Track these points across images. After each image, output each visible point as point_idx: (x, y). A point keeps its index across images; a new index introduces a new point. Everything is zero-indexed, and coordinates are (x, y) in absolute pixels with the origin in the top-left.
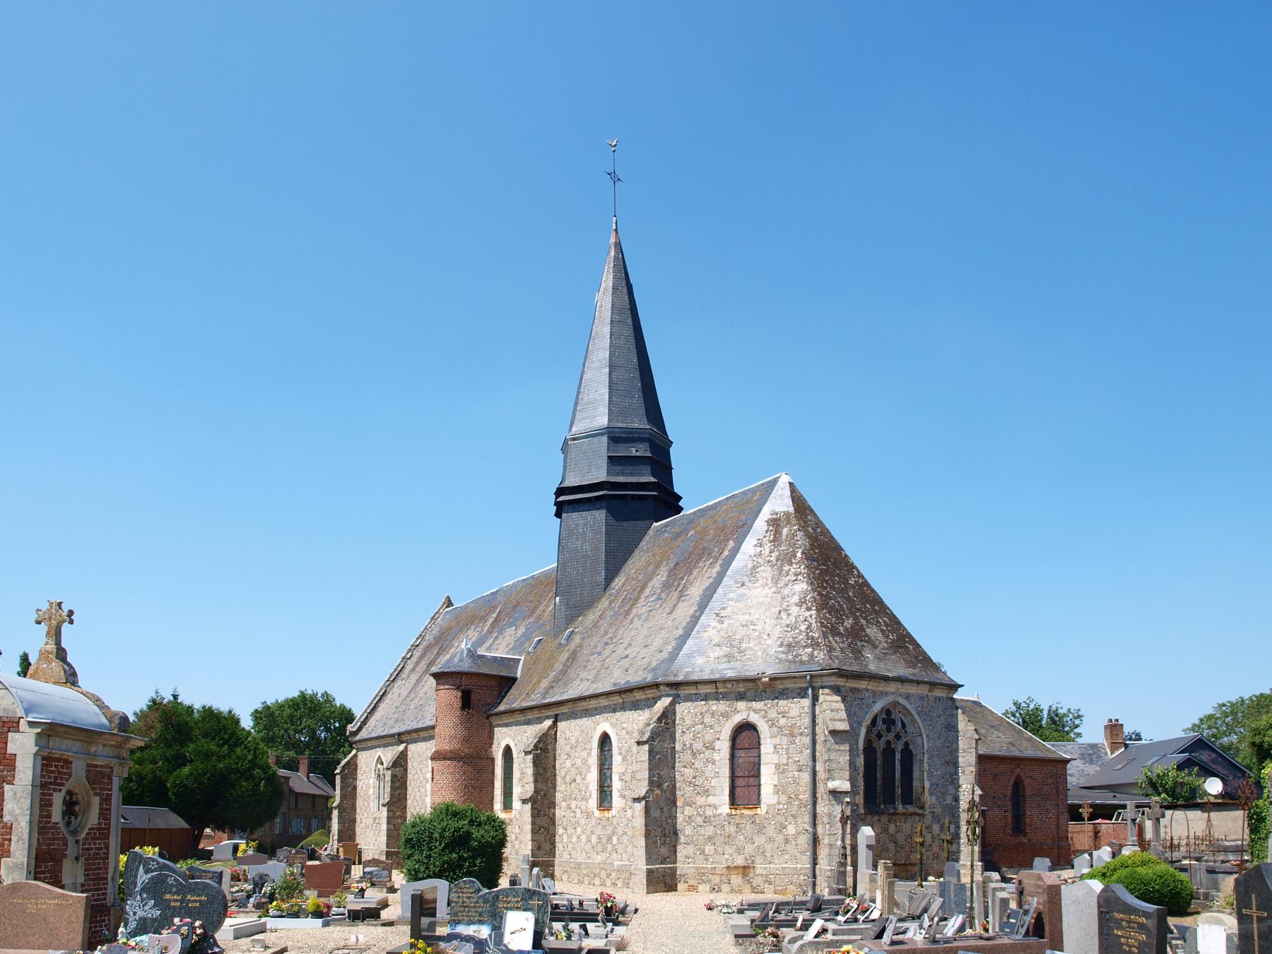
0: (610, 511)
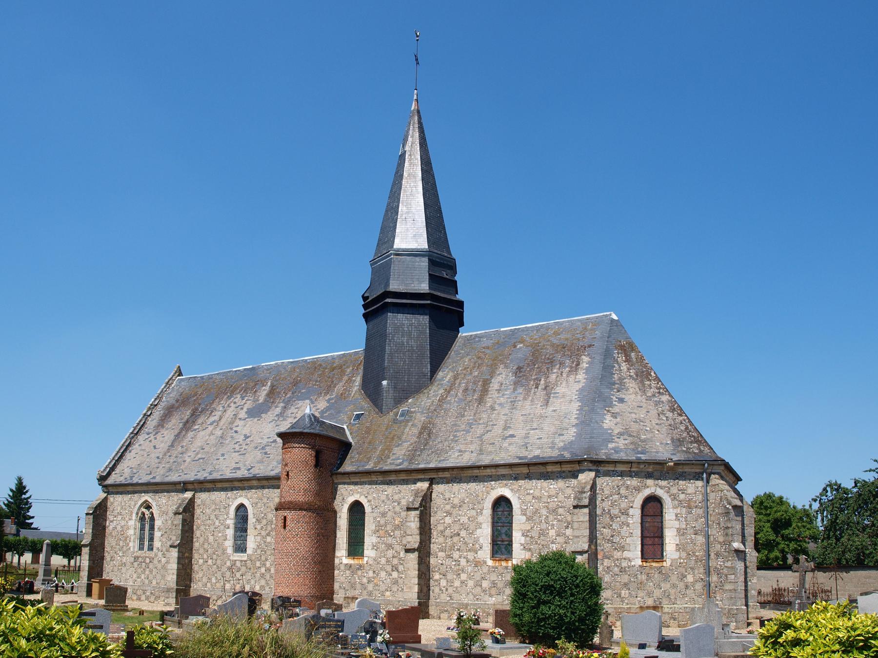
0: (432, 319)
